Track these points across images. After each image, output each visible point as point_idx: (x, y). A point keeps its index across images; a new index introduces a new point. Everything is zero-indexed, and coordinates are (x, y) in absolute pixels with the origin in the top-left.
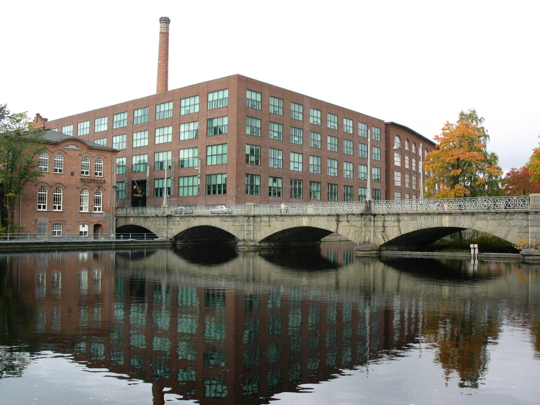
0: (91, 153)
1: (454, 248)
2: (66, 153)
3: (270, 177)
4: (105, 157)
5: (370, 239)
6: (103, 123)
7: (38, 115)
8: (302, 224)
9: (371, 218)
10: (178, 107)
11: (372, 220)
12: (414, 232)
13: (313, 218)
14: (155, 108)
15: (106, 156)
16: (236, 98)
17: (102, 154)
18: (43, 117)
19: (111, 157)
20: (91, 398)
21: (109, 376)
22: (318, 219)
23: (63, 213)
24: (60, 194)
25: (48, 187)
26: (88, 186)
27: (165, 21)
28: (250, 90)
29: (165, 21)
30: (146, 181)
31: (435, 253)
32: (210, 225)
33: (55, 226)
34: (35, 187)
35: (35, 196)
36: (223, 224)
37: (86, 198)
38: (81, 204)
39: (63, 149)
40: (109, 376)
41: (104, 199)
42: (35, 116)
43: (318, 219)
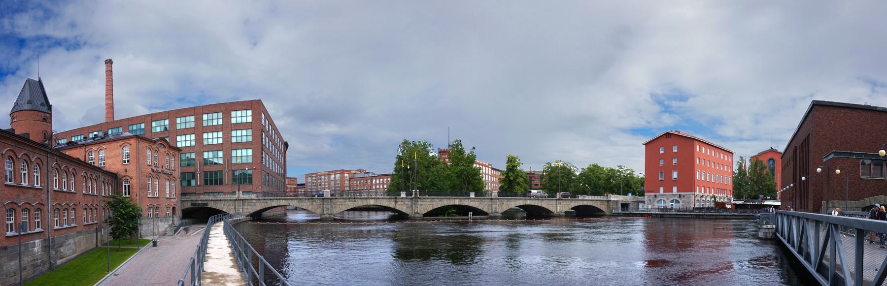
5: (418, 211)
34: (133, 179)
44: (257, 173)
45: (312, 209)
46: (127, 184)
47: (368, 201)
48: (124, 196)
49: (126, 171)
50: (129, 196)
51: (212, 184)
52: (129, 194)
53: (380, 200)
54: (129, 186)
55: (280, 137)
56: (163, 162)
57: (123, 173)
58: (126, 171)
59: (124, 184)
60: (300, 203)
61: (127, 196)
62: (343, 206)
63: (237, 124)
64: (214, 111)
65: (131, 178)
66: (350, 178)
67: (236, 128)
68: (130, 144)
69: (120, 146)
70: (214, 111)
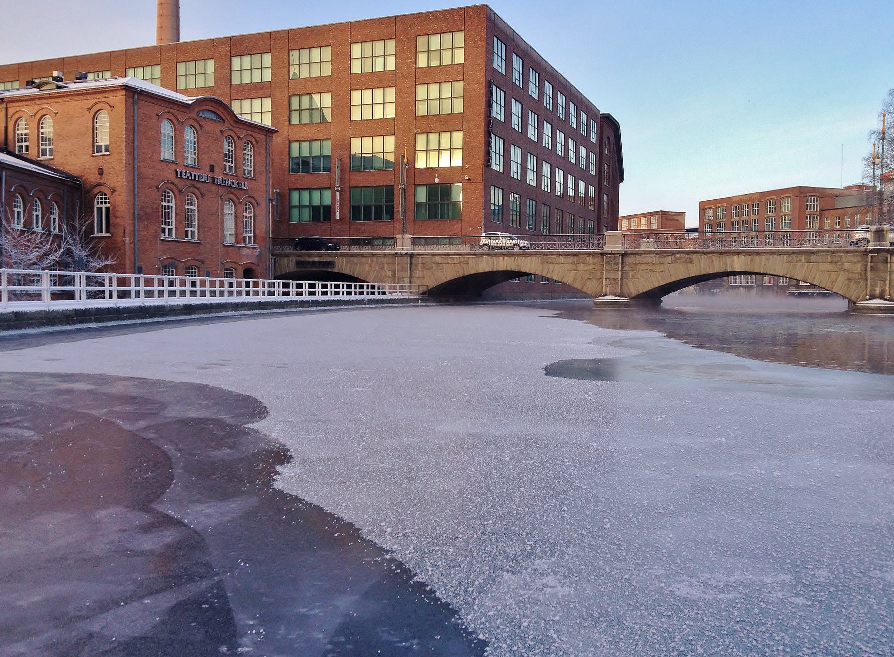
2: (201, 126)
8: (731, 266)
9: (887, 258)
10: (342, 58)
11: (889, 261)
12: (696, 276)
13: (758, 258)
15: (258, 139)
17: (253, 134)
20: (204, 606)
22: (768, 260)
23: (200, 246)
24: (192, 207)
25: (177, 192)
26: (235, 195)
31: (155, 304)
32: (476, 272)
34: (116, 193)
36: (549, 268)
39: (196, 117)
43: (768, 260)
44: (474, 191)
45: (574, 279)
46: (104, 206)
47: (728, 259)
48: (96, 234)
49: (101, 172)
50: (108, 235)
51: (436, 218)
52: (107, 231)
53: (764, 257)
54: (107, 209)
55: (583, 105)
56: (215, 156)
57: (93, 178)
58: (101, 172)
59: (96, 206)
60: (546, 265)
61: (104, 234)
62: (657, 274)
63: (429, 69)
64: (377, 38)
65: (114, 191)
66: (822, 210)
67: (261, 93)
68: (112, 107)
69: (90, 109)
70: (377, 38)
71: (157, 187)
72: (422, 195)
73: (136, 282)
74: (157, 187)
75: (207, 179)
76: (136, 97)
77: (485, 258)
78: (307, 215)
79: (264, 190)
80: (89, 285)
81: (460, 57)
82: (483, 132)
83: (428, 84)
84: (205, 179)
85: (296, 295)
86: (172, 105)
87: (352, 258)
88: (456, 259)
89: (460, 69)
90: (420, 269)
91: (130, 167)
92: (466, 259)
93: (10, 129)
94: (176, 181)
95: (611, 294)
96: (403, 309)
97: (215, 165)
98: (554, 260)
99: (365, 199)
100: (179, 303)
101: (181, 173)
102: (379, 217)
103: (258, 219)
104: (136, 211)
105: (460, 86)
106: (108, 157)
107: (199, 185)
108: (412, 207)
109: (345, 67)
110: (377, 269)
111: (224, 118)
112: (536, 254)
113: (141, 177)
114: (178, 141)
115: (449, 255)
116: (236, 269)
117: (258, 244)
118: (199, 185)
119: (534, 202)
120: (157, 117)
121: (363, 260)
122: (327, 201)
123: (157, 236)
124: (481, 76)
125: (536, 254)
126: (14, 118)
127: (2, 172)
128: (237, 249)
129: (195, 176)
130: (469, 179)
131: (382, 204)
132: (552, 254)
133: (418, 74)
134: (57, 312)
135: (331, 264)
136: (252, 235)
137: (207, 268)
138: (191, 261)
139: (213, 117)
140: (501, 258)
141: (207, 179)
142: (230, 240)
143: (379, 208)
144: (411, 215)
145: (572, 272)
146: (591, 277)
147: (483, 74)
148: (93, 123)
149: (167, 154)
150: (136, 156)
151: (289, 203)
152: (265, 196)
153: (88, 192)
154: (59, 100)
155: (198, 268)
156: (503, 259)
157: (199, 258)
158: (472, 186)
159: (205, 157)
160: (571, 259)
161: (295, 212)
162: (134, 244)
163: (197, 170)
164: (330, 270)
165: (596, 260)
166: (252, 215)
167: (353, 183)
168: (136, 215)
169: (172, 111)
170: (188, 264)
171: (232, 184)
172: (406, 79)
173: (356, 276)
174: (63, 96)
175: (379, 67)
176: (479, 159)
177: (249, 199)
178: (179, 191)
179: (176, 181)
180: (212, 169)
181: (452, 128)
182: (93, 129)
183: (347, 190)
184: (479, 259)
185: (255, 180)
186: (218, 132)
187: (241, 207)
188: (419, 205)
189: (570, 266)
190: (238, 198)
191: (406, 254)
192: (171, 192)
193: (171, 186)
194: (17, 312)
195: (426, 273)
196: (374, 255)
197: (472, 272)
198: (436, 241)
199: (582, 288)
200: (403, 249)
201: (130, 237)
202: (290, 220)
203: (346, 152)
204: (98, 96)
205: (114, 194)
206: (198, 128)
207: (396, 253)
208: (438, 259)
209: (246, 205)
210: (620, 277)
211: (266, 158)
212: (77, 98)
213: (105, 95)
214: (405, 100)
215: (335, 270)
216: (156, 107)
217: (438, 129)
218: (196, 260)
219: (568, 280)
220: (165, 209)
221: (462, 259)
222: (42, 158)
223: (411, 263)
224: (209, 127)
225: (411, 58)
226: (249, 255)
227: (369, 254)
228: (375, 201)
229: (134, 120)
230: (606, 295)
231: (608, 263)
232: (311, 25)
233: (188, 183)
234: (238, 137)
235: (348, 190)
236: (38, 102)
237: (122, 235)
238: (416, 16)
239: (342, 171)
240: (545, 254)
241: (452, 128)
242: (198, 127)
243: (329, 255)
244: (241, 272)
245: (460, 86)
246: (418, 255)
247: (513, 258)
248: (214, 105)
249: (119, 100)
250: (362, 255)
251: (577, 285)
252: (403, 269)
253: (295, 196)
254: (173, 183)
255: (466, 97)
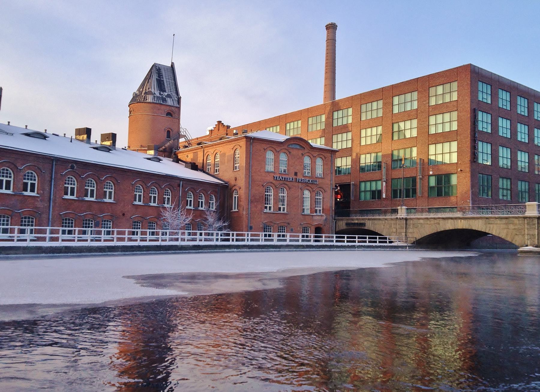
0: (312, 153)
1: (157, 276)
2: (290, 153)
3: (500, 177)
4: (325, 157)
6: (319, 121)
7: (219, 122)
14: (359, 108)
16: (469, 91)
17: (322, 153)
18: (225, 124)
19: (330, 158)
21: (17, 363)
23: (288, 215)
26: (310, 187)
27: (332, 28)
28: (482, 82)
29: (332, 28)
30: (350, 184)
32: (470, 228)
33: (280, 228)
35: (263, 196)
37: (308, 199)
38: (316, 207)
39: (287, 148)
40: (17, 363)
41: (324, 201)
42: (217, 123)
51: (441, 195)
57: (233, 182)
60: (489, 225)
65: (240, 188)
71: (263, 185)
72: (433, 182)
73: (248, 235)
74: (263, 185)
75: (293, 179)
76: (252, 141)
77: (450, 221)
78: (368, 195)
79: (330, 183)
80: (237, 236)
81: (455, 97)
82: (470, 141)
83: (436, 115)
84: (291, 180)
85: (336, 242)
86: (273, 143)
87: (374, 221)
88: (433, 222)
89: (455, 104)
90: (412, 227)
91: (248, 176)
92: (438, 221)
93: (205, 159)
94: (274, 182)
95: (531, 245)
96: (361, 251)
97: (297, 171)
98: (493, 222)
99: (401, 185)
100: (190, 244)
101: (276, 177)
102: (408, 196)
103: (325, 200)
104: (250, 198)
105: (455, 115)
106: (238, 172)
107: (287, 183)
108: (427, 189)
109: (389, 110)
110: (388, 227)
111: (304, 147)
112: (481, 218)
113: (253, 181)
114: (277, 161)
115: (428, 219)
116: (310, 228)
117: (325, 214)
118: (287, 183)
119: (527, 184)
120: (264, 150)
121: (381, 222)
122: (379, 188)
123: (262, 210)
124: (467, 106)
125: (481, 218)
126: (206, 155)
127: (180, 182)
128: (311, 217)
129: (285, 178)
130: (461, 170)
131: (409, 188)
132: (491, 218)
133: (430, 110)
134: (95, 247)
135: (364, 224)
136: (321, 209)
137: (291, 227)
138: (306, 224)
139: (298, 147)
140: (460, 221)
141: (293, 179)
142: (307, 212)
143: (408, 191)
144: (426, 194)
145: (505, 230)
146: (518, 233)
147: (469, 105)
148: (234, 155)
149: (270, 167)
150: (250, 170)
151: (360, 190)
152: (330, 187)
153: (231, 189)
154: (222, 145)
155: (286, 227)
156: (461, 221)
157: (287, 221)
158: (463, 175)
159: (292, 168)
160: (504, 221)
161: (363, 194)
162: (248, 215)
163: (287, 176)
164: (363, 228)
165: (521, 222)
166: (322, 198)
167: (394, 177)
168: (250, 200)
169: (273, 146)
170: (280, 225)
171: (308, 181)
172: (423, 113)
173: (376, 231)
174: (223, 143)
175: (408, 108)
176: (467, 157)
177: (319, 189)
178: (276, 187)
179: (274, 182)
180: (296, 174)
181: (450, 140)
182: (234, 158)
183: (390, 180)
184: (446, 221)
185: (324, 178)
186: (300, 155)
187: (314, 194)
188: (432, 188)
189: (504, 226)
190: (312, 189)
191: (403, 218)
192: (271, 187)
193: (270, 184)
194: (66, 246)
195: (415, 230)
196: (386, 219)
197: (442, 230)
198: (438, 210)
199: (512, 240)
200: (401, 216)
201: (246, 211)
202: (360, 198)
203: (389, 159)
204: (236, 142)
205: (241, 190)
206: (288, 153)
207: (397, 218)
208: (421, 221)
209: (318, 192)
210: (537, 234)
211: (331, 166)
212: (228, 144)
213: (239, 141)
214: (422, 125)
215: (366, 228)
216: (263, 145)
217: (442, 141)
218: (285, 223)
219: (503, 235)
220: (266, 196)
221: (436, 221)
222: (216, 173)
223: (406, 224)
224: (294, 152)
225: (426, 101)
226: (319, 219)
227: (383, 219)
228: (406, 187)
229: (250, 152)
230: (527, 246)
231: (528, 224)
232: (372, 90)
233: (281, 182)
234: (313, 156)
235: (390, 181)
236: (214, 147)
237: (242, 210)
238: (429, 76)
239: (387, 170)
240: (487, 218)
241: (450, 140)
242: (288, 153)
243: (363, 219)
244: (313, 229)
245: (455, 115)
246: (410, 219)
247: (467, 221)
248: (298, 141)
249: (243, 143)
250: (379, 219)
251: (509, 239)
252: (402, 228)
253: (363, 185)
254: (272, 183)
255: (459, 120)
